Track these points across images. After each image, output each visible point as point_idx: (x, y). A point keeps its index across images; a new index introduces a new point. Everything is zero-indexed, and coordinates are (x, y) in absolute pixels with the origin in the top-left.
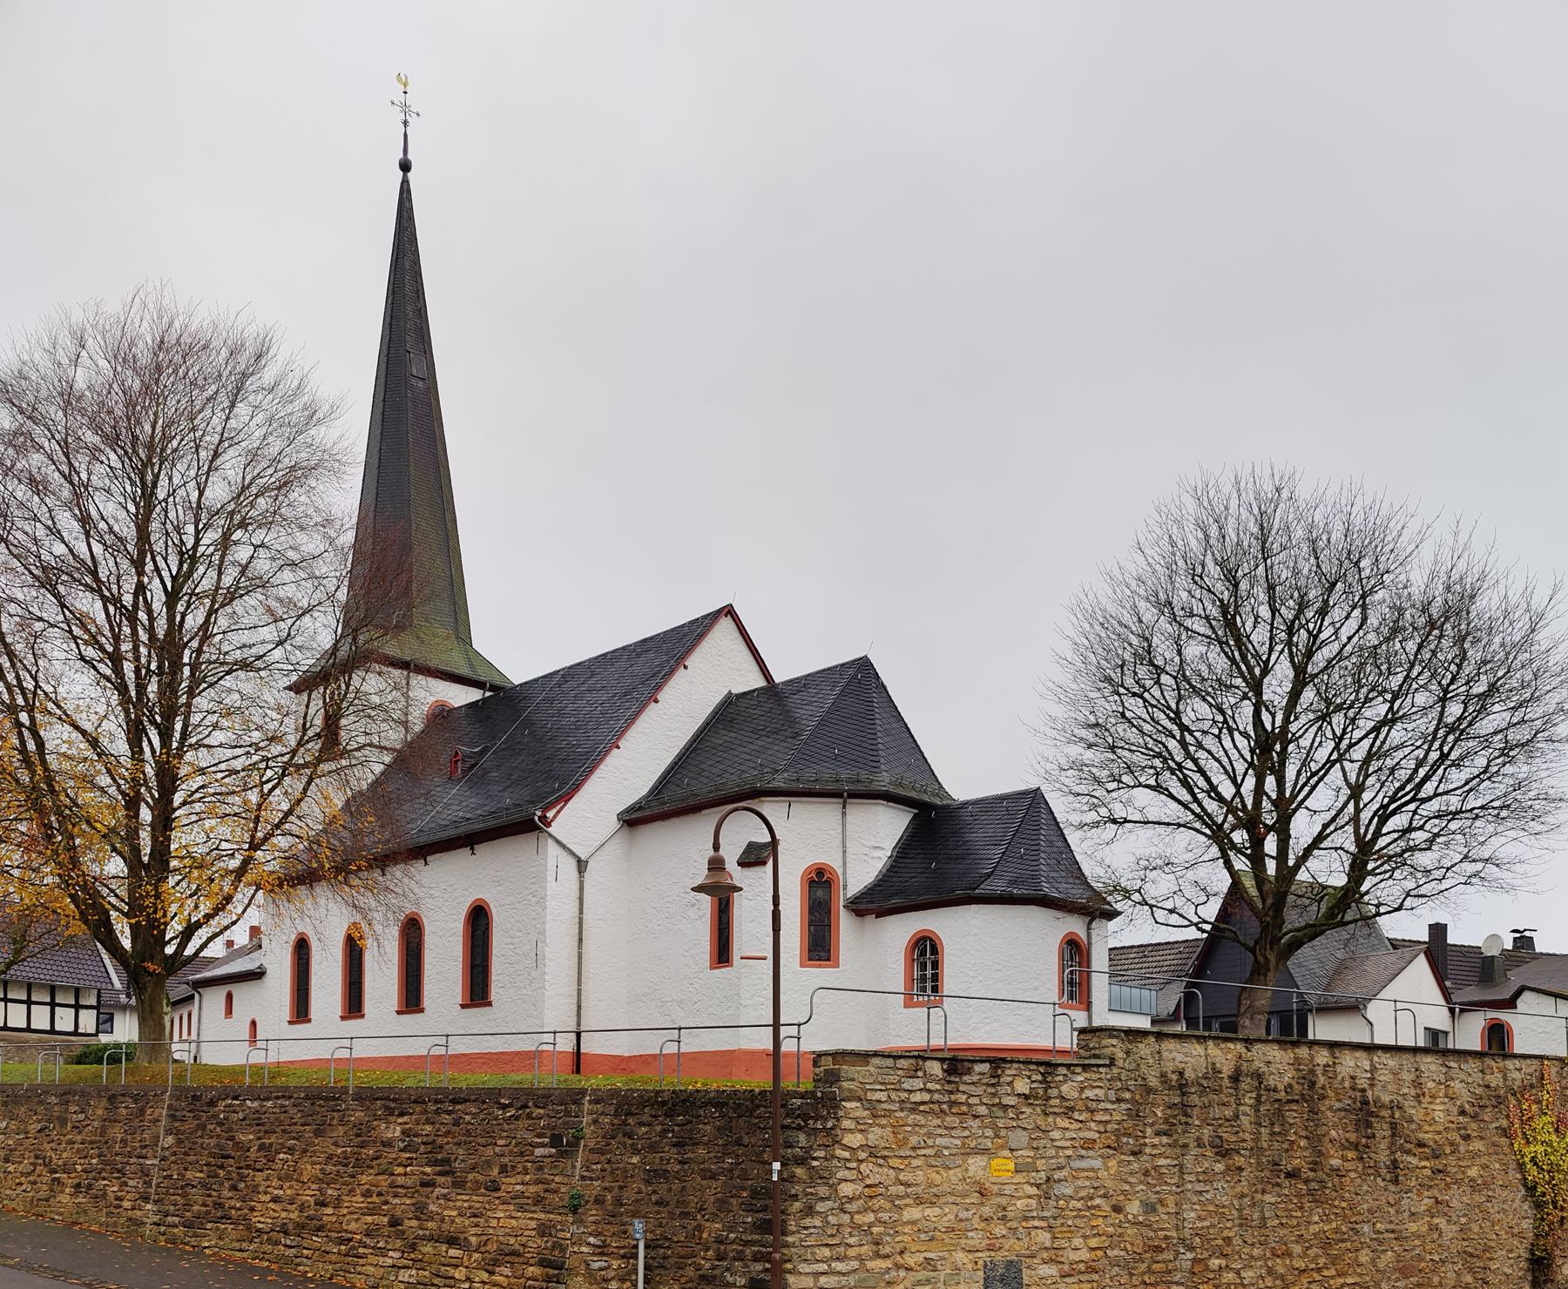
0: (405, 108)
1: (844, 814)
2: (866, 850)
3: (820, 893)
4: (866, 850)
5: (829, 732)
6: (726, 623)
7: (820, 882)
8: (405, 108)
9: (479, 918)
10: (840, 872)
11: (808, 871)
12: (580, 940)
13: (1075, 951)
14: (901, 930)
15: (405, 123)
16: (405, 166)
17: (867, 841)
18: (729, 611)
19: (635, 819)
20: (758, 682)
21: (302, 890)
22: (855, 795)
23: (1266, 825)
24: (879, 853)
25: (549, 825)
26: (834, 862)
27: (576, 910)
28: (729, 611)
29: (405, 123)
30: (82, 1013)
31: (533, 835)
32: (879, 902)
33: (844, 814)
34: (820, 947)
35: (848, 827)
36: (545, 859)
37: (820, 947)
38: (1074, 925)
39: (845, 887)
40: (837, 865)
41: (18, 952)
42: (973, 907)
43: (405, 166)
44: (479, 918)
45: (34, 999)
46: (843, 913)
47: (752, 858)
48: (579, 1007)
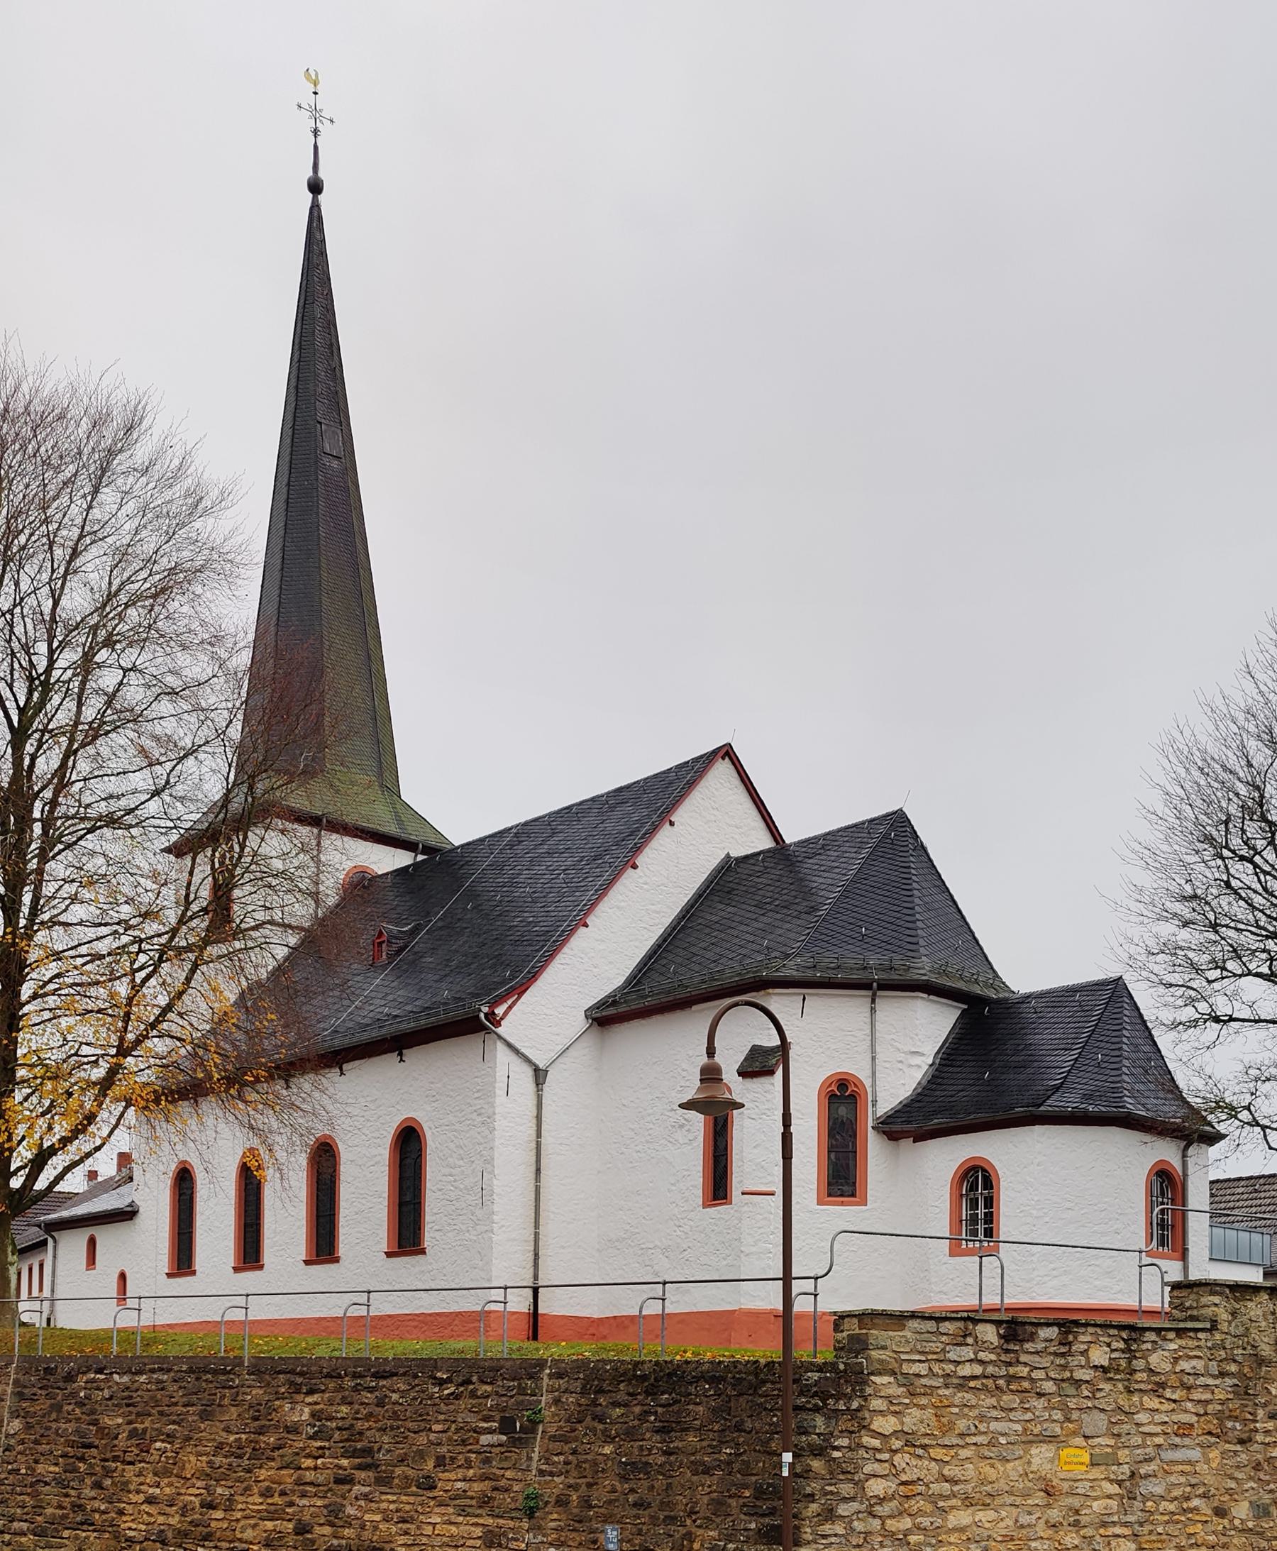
0: (315, 113)
1: (873, 1010)
2: (901, 1057)
3: (842, 1111)
4: (901, 1057)
6: (722, 768)
7: (842, 1097)
8: (315, 113)
9: (409, 1143)
10: (867, 1083)
11: (827, 1083)
12: (538, 1170)
13: (1167, 1184)
14: (944, 1158)
15: (316, 132)
16: (315, 187)
17: (903, 1045)
18: (727, 752)
19: (608, 1016)
20: (766, 843)
21: (185, 1107)
24: (917, 1060)
25: (498, 1024)
26: (858, 1068)
27: (533, 1132)
28: (727, 752)
29: (316, 132)
31: (475, 1040)
32: (916, 1122)
33: (873, 1010)
34: (842, 1179)
35: (879, 1026)
36: (494, 1068)
37: (842, 1179)
38: (1167, 1151)
40: (864, 1076)
42: (1038, 1129)
43: (315, 187)
44: (409, 1143)
46: (871, 1134)
47: (757, 1066)
48: (536, 1255)
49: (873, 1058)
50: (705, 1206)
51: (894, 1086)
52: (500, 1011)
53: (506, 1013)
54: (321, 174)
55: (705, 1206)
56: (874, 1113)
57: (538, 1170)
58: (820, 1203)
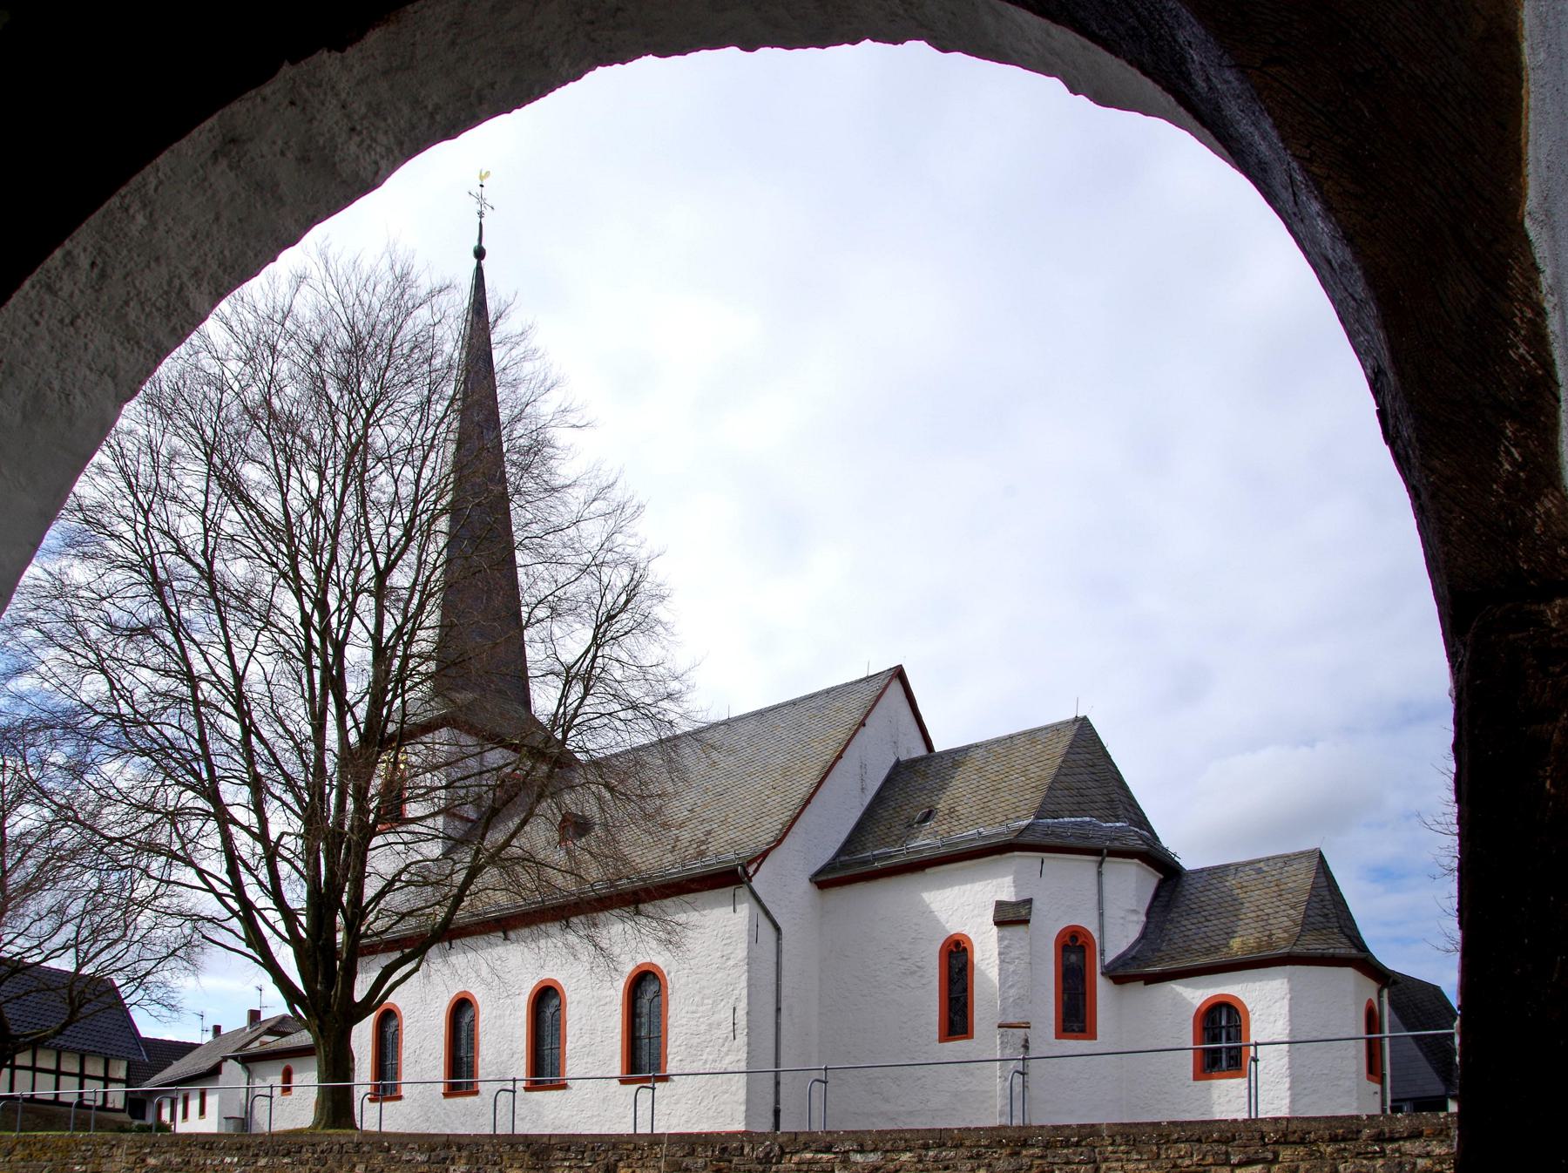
0: (481, 199)
1: (1100, 874)
3: (1073, 958)
5: (1078, 797)
7: (1074, 948)
8: (481, 199)
10: (1096, 936)
15: (481, 215)
16: (480, 253)
19: (829, 879)
20: (921, 751)
21: (554, 928)
22: (1115, 853)
23: (258, 1051)
24: (1135, 918)
28: (899, 674)
29: (481, 215)
30: (18, 1073)
31: (730, 890)
32: (1134, 971)
33: (1100, 874)
34: (1075, 1016)
35: (1107, 888)
37: (1075, 1016)
39: (1102, 954)
40: (1092, 928)
41: (73, 1013)
43: (480, 253)
45: (63, 1069)
46: (1455, 1002)
49: (1101, 915)
50: (941, 1041)
51: (1120, 933)
52: (751, 870)
53: (756, 871)
54: (484, 245)
55: (941, 1041)
56: (1102, 960)
57: (778, 1010)
58: (1057, 1037)
